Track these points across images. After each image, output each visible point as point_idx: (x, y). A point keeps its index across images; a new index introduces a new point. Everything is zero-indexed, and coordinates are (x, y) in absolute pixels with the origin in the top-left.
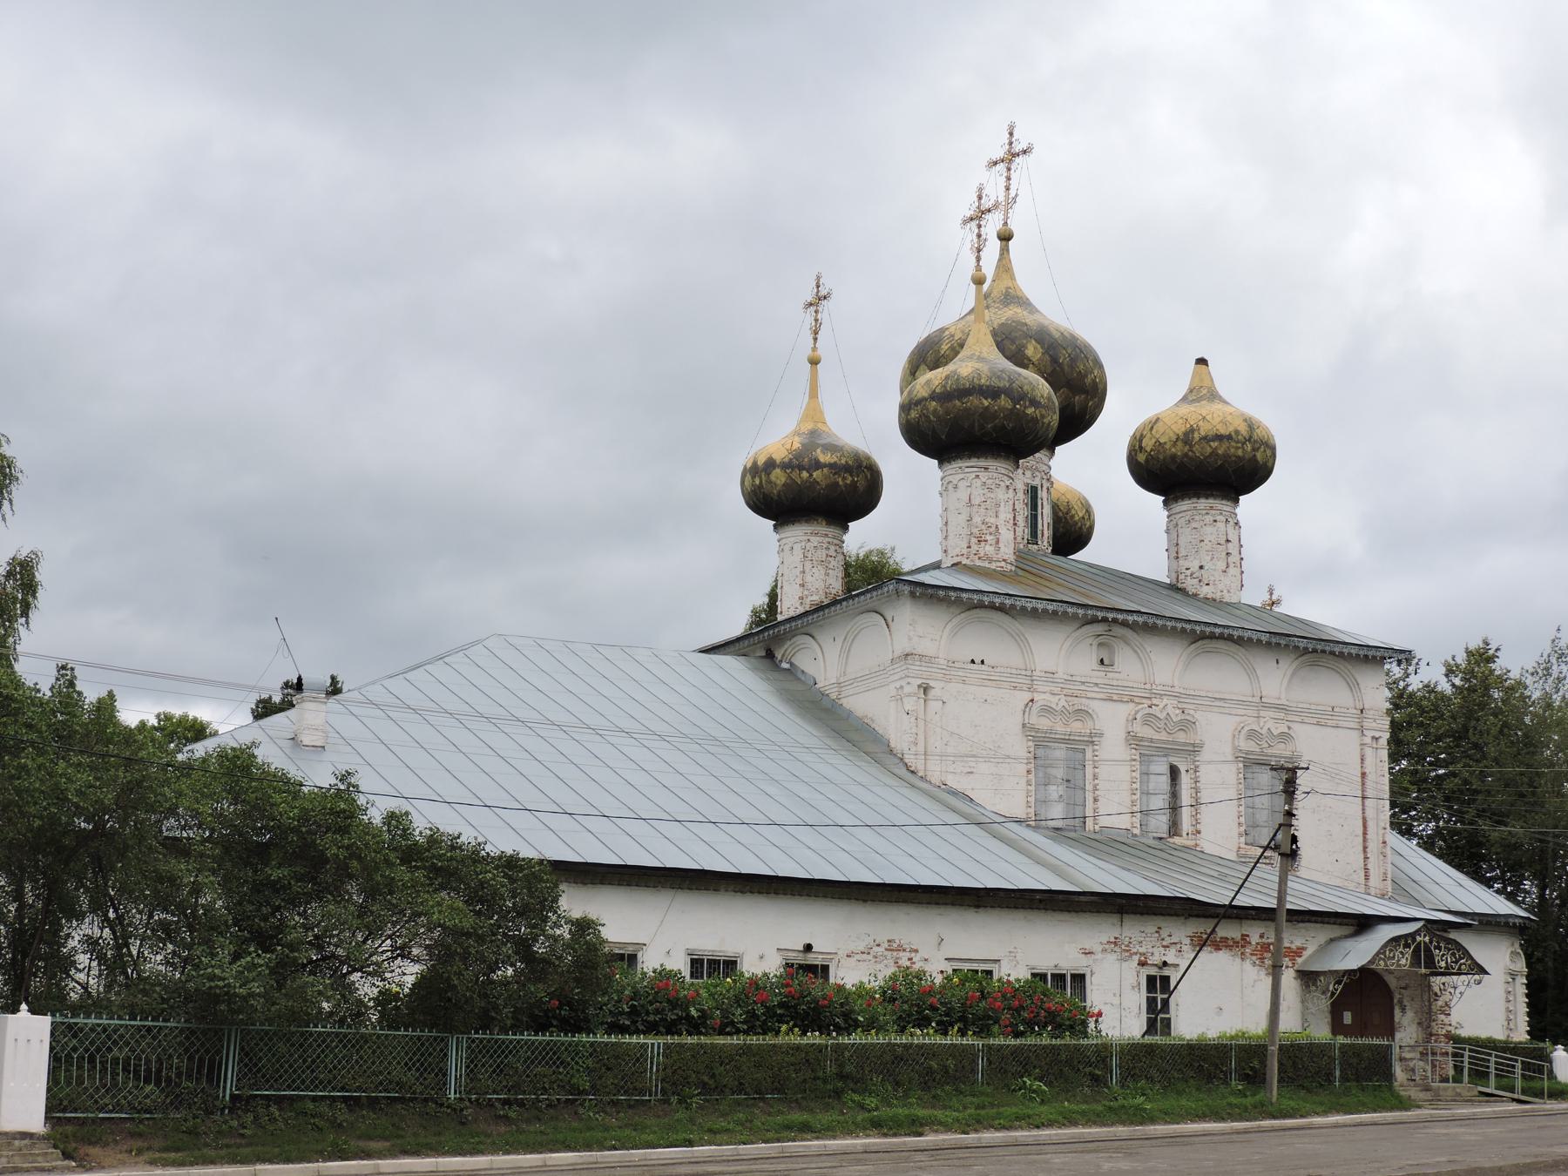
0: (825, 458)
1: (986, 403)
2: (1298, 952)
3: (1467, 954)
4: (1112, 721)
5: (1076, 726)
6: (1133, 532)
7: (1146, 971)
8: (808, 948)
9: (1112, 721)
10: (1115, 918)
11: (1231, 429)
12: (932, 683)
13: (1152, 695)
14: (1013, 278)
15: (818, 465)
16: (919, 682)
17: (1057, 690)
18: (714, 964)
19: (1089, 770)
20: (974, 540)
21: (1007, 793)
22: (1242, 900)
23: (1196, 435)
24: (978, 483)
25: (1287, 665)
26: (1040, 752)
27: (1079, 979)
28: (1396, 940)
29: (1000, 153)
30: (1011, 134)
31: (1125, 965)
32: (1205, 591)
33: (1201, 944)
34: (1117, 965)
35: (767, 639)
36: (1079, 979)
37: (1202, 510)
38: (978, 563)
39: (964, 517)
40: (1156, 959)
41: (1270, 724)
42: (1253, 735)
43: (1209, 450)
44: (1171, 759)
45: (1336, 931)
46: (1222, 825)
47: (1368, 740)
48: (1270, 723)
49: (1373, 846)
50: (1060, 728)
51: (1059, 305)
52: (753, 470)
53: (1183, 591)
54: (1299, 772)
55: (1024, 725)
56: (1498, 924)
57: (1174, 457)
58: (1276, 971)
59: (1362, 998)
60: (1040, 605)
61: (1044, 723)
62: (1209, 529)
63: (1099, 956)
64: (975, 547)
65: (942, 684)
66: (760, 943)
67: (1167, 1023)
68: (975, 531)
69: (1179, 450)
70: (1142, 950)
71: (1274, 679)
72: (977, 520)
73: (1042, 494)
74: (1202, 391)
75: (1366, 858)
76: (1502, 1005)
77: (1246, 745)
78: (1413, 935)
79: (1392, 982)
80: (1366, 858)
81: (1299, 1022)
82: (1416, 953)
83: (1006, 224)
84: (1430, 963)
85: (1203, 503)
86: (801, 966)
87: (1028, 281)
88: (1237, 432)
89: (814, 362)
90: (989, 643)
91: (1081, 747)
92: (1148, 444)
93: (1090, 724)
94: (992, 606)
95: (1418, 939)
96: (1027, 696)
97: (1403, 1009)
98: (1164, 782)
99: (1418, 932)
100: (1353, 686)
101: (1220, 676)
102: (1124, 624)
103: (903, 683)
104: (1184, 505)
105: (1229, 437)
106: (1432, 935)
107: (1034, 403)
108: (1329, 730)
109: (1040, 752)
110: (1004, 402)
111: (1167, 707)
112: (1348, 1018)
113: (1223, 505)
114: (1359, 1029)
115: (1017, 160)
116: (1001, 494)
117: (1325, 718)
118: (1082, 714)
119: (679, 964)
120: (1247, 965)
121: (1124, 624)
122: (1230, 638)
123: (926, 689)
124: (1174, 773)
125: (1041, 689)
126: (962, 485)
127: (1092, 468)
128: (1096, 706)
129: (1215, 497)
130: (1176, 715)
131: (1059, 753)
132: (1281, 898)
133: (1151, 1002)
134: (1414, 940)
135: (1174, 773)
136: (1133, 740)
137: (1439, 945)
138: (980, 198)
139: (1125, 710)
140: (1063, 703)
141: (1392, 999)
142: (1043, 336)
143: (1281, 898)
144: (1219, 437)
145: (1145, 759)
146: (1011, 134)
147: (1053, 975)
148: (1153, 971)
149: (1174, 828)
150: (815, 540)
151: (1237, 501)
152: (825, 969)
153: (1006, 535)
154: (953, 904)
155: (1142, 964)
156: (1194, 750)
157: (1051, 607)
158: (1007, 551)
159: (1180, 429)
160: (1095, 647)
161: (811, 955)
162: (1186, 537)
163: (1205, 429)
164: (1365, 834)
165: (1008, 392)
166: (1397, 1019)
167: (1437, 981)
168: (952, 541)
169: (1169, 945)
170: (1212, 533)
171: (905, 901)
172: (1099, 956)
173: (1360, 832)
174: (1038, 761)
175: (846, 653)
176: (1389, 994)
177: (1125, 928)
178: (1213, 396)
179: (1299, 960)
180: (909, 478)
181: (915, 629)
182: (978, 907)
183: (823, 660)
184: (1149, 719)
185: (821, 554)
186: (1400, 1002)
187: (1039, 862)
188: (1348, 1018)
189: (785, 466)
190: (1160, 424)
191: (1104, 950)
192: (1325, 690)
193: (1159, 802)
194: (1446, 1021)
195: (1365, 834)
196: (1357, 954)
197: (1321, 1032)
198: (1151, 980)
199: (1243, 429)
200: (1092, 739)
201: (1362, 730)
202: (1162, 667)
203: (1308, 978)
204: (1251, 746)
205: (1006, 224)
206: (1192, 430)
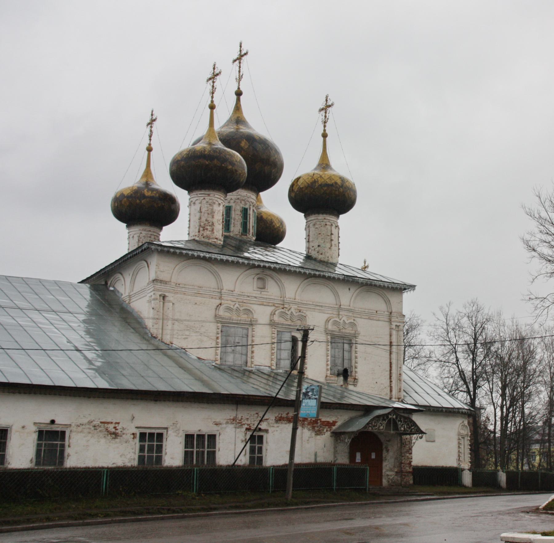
0: (147, 193)
1: (207, 163)
2: (334, 423)
3: (415, 424)
4: (262, 314)
8: (53, 422)
9: (262, 314)
10: (234, 407)
11: (333, 182)
12: (167, 294)
14: (242, 113)
15: (144, 196)
16: (160, 293)
17: (234, 300)
20: (201, 229)
23: (317, 184)
24: (204, 202)
26: (224, 329)
27: (212, 438)
28: (378, 417)
29: (236, 56)
30: (241, 46)
31: (238, 430)
32: (320, 257)
34: (234, 429)
35: (101, 283)
36: (212, 438)
38: (203, 239)
39: (198, 217)
41: (344, 318)
43: (322, 191)
44: (293, 334)
45: (353, 414)
47: (394, 327)
48: (345, 318)
49: (137, 298)
50: (235, 318)
51: (258, 125)
54: (310, 331)
55: (216, 316)
56: (454, 412)
62: (323, 228)
63: (224, 426)
64: (202, 232)
65: (173, 295)
67: (260, 459)
68: (202, 224)
70: (249, 422)
71: (347, 296)
72: (203, 219)
75: (391, 381)
76: (456, 450)
77: (330, 327)
78: (387, 415)
79: (382, 438)
80: (391, 381)
81: (332, 456)
83: (239, 88)
84: (396, 428)
86: (47, 432)
87: (247, 113)
88: (336, 183)
90: (196, 276)
92: (296, 188)
93: (251, 316)
95: (390, 416)
96: (218, 302)
97: (388, 451)
99: (389, 413)
101: (322, 295)
102: (269, 268)
103: (152, 293)
104: (312, 217)
105: (332, 185)
108: (375, 322)
109: (224, 329)
115: (243, 58)
117: (371, 316)
118: (248, 311)
122: (324, 277)
123: (164, 297)
125: (225, 298)
126: (197, 202)
127: (275, 201)
129: (326, 213)
131: (233, 331)
133: (252, 450)
134: (388, 417)
138: (214, 69)
139: (270, 309)
140: (237, 305)
141: (382, 447)
142: (251, 139)
144: (327, 185)
146: (241, 46)
147: (198, 435)
150: (144, 233)
151: (338, 217)
152: (63, 433)
154: (141, 399)
155: (248, 429)
159: (309, 181)
160: (256, 280)
161: (53, 426)
163: (320, 181)
164: (391, 370)
165: (217, 158)
166: (384, 456)
168: (191, 230)
171: (114, 398)
172: (224, 426)
173: (388, 369)
175: (133, 282)
176: (381, 444)
177: (238, 412)
179: (334, 428)
180: (182, 196)
182: (156, 401)
183: (123, 286)
186: (386, 448)
190: (301, 179)
191: (227, 423)
194: (410, 456)
195: (391, 370)
196: (360, 424)
199: (339, 182)
201: (390, 321)
203: (337, 435)
204: (335, 328)
205: (239, 88)
206: (315, 182)
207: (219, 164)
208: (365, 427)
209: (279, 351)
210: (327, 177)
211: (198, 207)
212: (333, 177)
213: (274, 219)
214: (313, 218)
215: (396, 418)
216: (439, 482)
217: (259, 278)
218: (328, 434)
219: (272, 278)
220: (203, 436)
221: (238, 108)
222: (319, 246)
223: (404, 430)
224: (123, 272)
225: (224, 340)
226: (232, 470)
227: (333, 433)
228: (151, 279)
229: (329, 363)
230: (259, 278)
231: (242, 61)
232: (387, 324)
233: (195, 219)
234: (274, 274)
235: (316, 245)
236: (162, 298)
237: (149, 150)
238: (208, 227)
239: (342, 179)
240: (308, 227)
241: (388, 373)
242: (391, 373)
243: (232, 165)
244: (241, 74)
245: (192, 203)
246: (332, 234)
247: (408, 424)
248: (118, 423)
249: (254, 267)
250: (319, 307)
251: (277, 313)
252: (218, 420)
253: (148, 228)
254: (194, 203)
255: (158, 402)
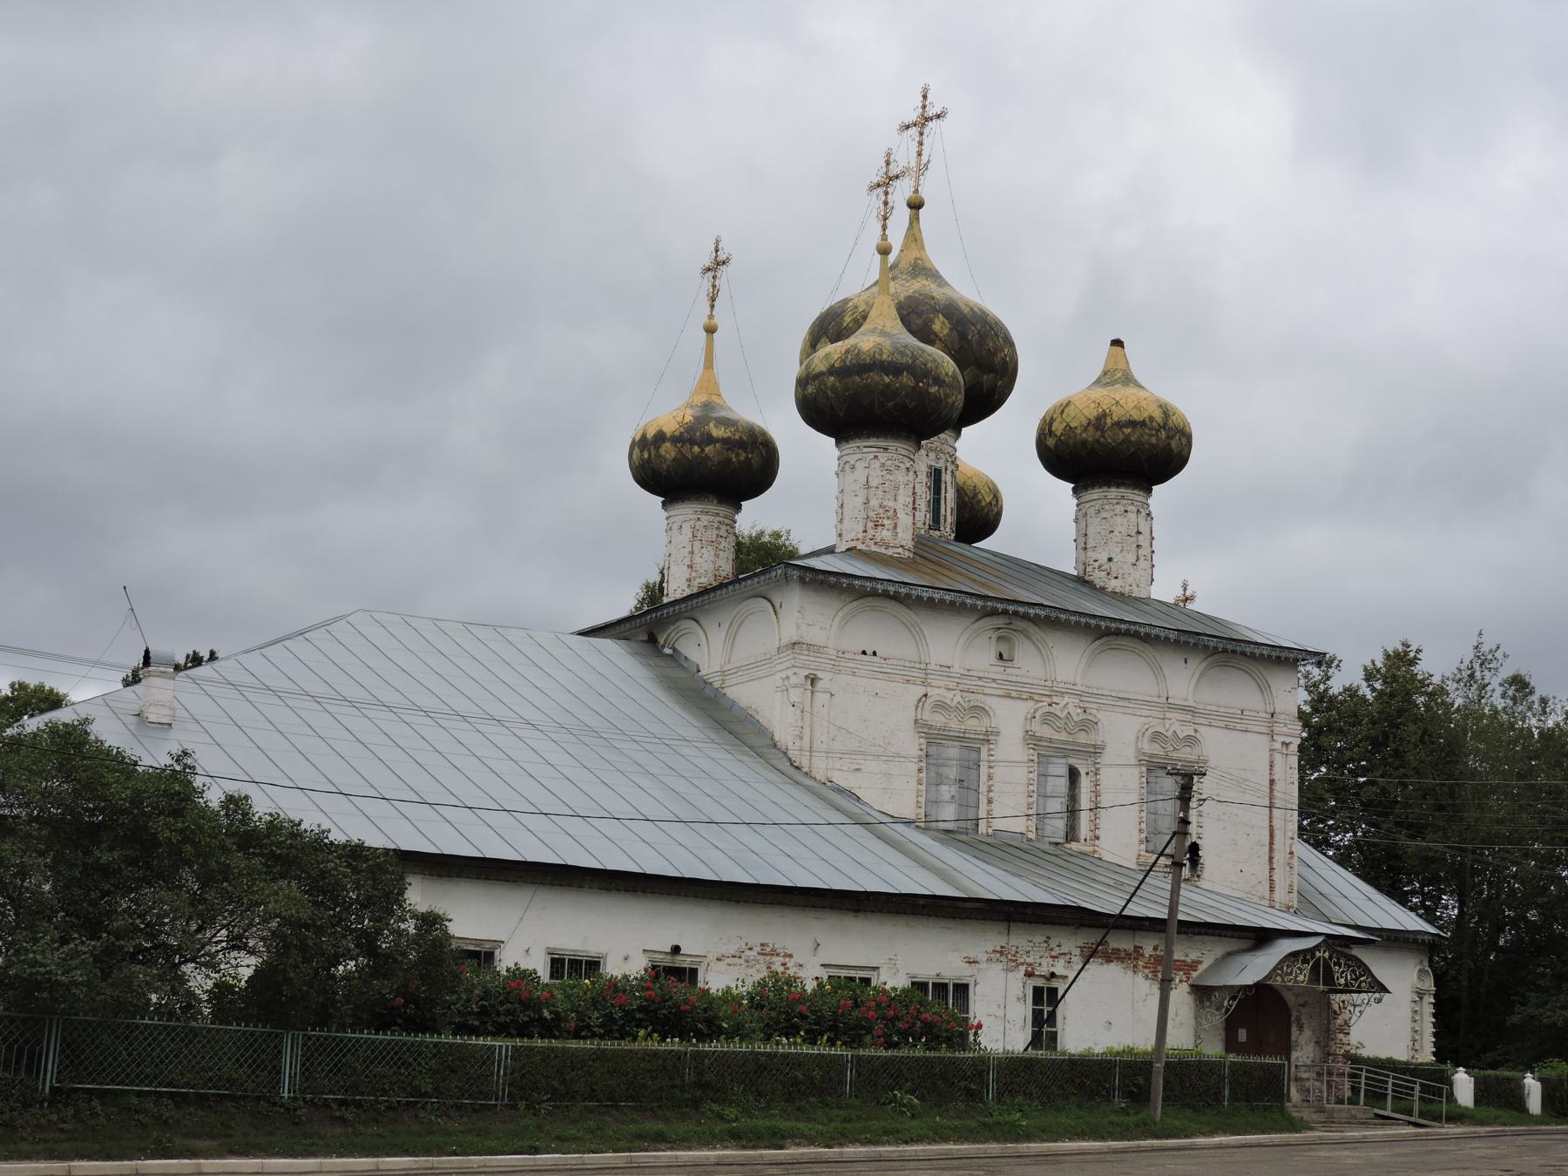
0: (718, 432)
1: (887, 380)
2: (1194, 965)
4: (1010, 720)
5: (972, 724)
6: (1041, 519)
7: (1033, 982)
8: (676, 950)
9: (1010, 720)
10: (1002, 927)
11: (1145, 415)
12: (819, 674)
13: (1053, 693)
14: (922, 248)
15: (710, 439)
17: (952, 685)
18: (575, 964)
19: (984, 770)
20: (870, 524)
21: (896, 792)
22: (1135, 910)
23: (1109, 421)
24: (877, 464)
25: (1196, 665)
26: (933, 750)
27: (962, 989)
28: (1294, 955)
29: (913, 116)
30: (925, 97)
32: (1113, 585)
33: (1089, 955)
34: (1003, 975)
37: (1113, 501)
38: (874, 548)
39: (861, 499)
40: (1044, 970)
42: (1156, 737)
43: (1121, 436)
44: (1071, 761)
45: (1233, 945)
46: (1120, 832)
47: (1277, 745)
48: (1176, 726)
49: (746, 678)
50: (954, 725)
51: (968, 284)
52: (641, 444)
53: (1089, 584)
55: (916, 721)
57: (1084, 442)
58: (1165, 986)
59: (1258, 1015)
60: (937, 596)
61: (937, 720)
62: (1119, 520)
64: (871, 532)
65: (830, 676)
66: (624, 943)
67: (1053, 1037)
68: (872, 514)
69: (1090, 435)
70: (1029, 960)
71: (1182, 679)
72: (874, 503)
73: (947, 478)
74: (1117, 375)
75: (1272, 869)
76: (1408, 1024)
78: (1312, 951)
79: (1290, 999)
80: (1272, 869)
81: (1192, 1038)
82: (1315, 968)
83: (916, 191)
84: (1329, 979)
85: (1114, 492)
87: (938, 254)
88: (1151, 418)
89: (710, 330)
90: (882, 633)
91: (975, 746)
92: (1058, 427)
94: (886, 595)
96: (921, 691)
97: (1301, 1028)
98: (1062, 785)
99: (1317, 947)
100: (1265, 688)
102: (1025, 617)
103: (789, 673)
104: (1095, 494)
106: (1333, 952)
107: (938, 381)
109: (933, 750)
110: (906, 379)
111: (1068, 706)
112: (1242, 1035)
113: (1135, 495)
114: (1255, 1046)
115: (931, 124)
116: (900, 477)
117: (1233, 722)
118: (978, 711)
119: (540, 966)
120: (1140, 978)
121: (1025, 617)
123: (813, 680)
124: (1073, 775)
125: (935, 683)
126: (860, 465)
127: (997, 450)
128: (991, 703)
130: (1077, 714)
131: (952, 751)
132: (1173, 907)
134: (1313, 955)
135: (1073, 775)
136: (1032, 740)
137: (1340, 961)
139: (1024, 708)
142: (952, 311)
143: (1173, 907)
144: (1132, 423)
145: (1043, 760)
146: (925, 97)
148: (1040, 983)
149: (1071, 833)
150: (705, 519)
153: (905, 520)
155: (1029, 975)
156: (1095, 751)
157: (948, 597)
158: (905, 537)
159: (1092, 413)
160: (994, 640)
162: (1095, 527)
164: (1271, 843)
166: (1293, 1038)
167: (1337, 999)
169: (1057, 955)
170: (1122, 524)
172: (984, 966)
174: (929, 759)
175: (731, 639)
178: (1128, 380)
179: (1194, 974)
180: (806, 453)
181: (801, 616)
183: (706, 648)
184: (1049, 718)
185: (712, 534)
186: (1298, 1020)
187: (924, 865)
188: (1242, 1035)
189: (675, 440)
190: (1071, 407)
192: (1235, 692)
193: (1057, 805)
194: (1345, 1040)
195: (1271, 843)
196: (1254, 969)
197: (1213, 1049)
198: (1038, 992)
199: (1158, 415)
200: (988, 738)
202: (1064, 664)
203: (1202, 993)
205: (916, 191)
206: (1104, 415)
207: (911, 382)
208: (1268, 977)
209: (1041, 800)
210: (1131, 405)
211: (860, 475)
212: (1144, 404)
213: (980, 487)
214: (1095, 496)
215: (1331, 957)
216: (1383, 1088)
217: (1000, 638)
218: (1185, 987)
219: (1028, 637)
220: (945, 986)
221: (913, 235)
222: (1110, 560)
223: (1346, 985)
224: (701, 619)
225: (932, 774)
226: (1015, 1071)
227: (1192, 986)
228: (785, 641)
229: (1143, 826)
230: (1000, 638)
231: (926, 131)
232: (1266, 738)
233: (854, 504)
234: (1031, 628)
235: (1103, 557)
236: (1170, 785)
237: (710, 330)
238: (886, 522)
239: (1166, 411)
240: (1081, 518)
241: (1267, 849)
242: (1271, 850)
243: (909, 382)
244: (924, 159)
245: (847, 467)
246: (1139, 533)
247: (1353, 971)
248: (791, 956)
249: (993, 613)
250: (1123, 701)
251: (1038, 715)
252: (972, 955)
253: (713, 507)
254: (853, 467)
255: (861, 915)
